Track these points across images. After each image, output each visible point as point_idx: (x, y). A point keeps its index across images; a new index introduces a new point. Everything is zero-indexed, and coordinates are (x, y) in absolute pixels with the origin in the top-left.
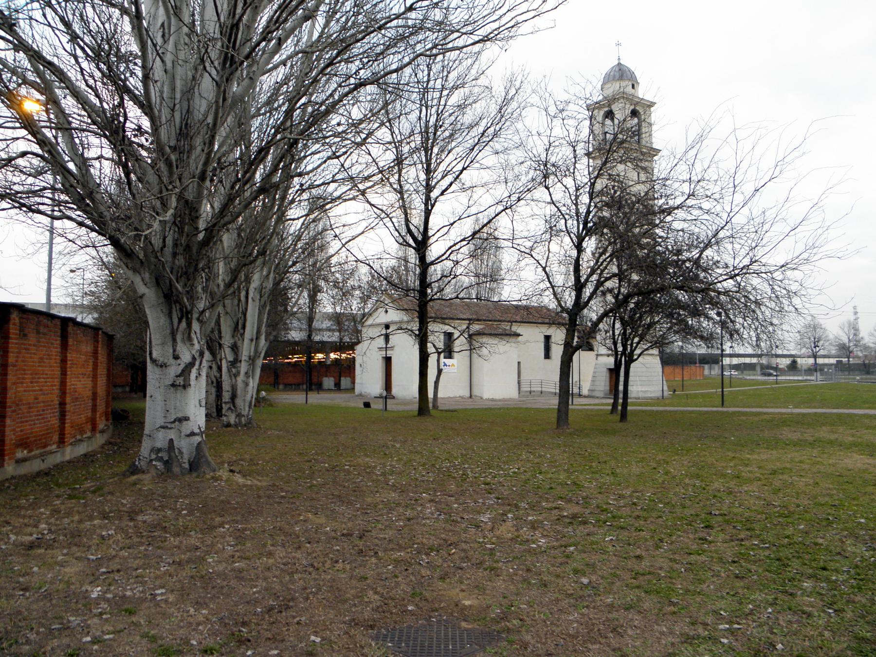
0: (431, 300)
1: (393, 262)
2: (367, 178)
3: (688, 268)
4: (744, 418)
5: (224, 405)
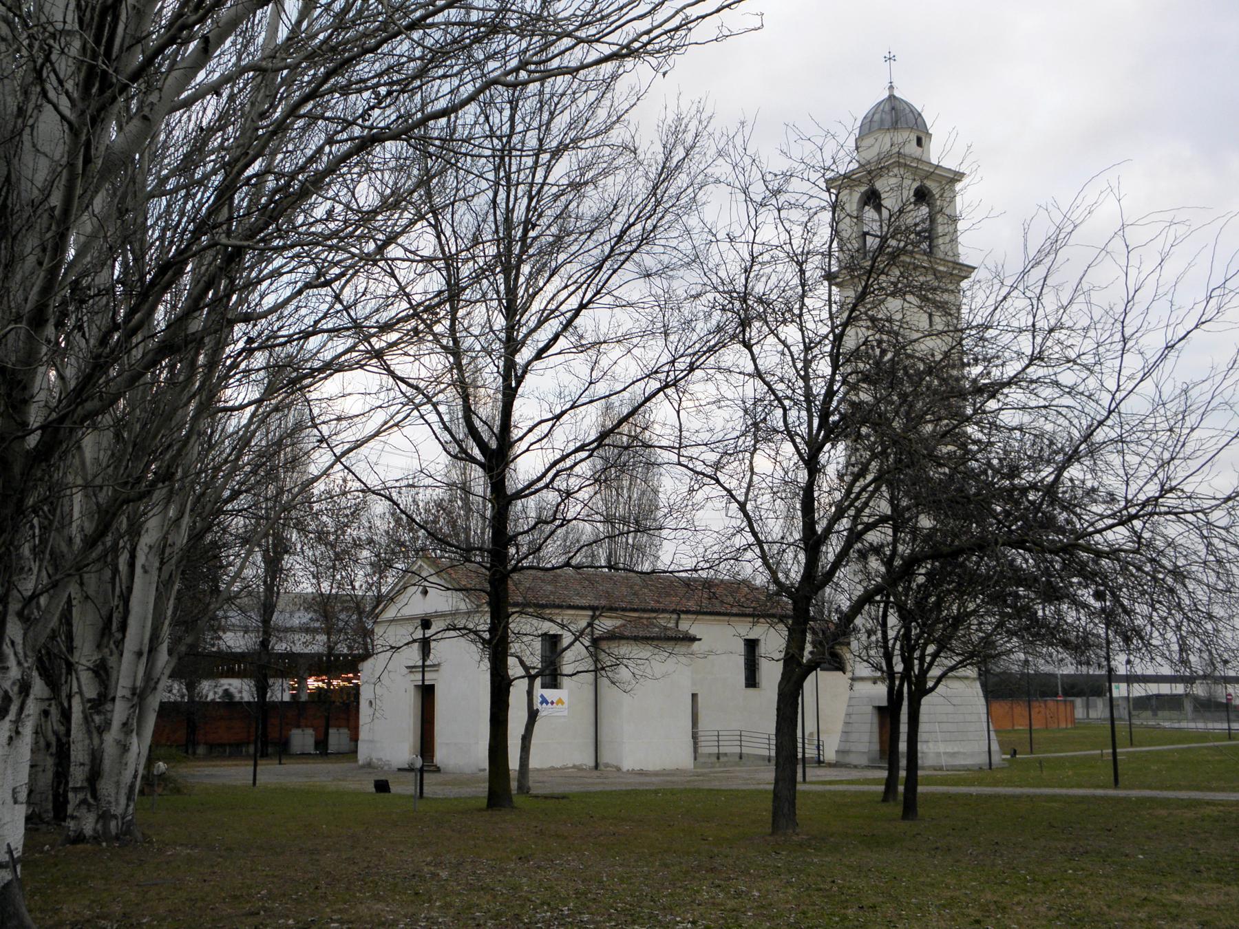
0: (516, 569)
1: (439, 493)
2: (386, 328)
3: (1032, 503)
4: (1164, 812)
5: (71, 795)
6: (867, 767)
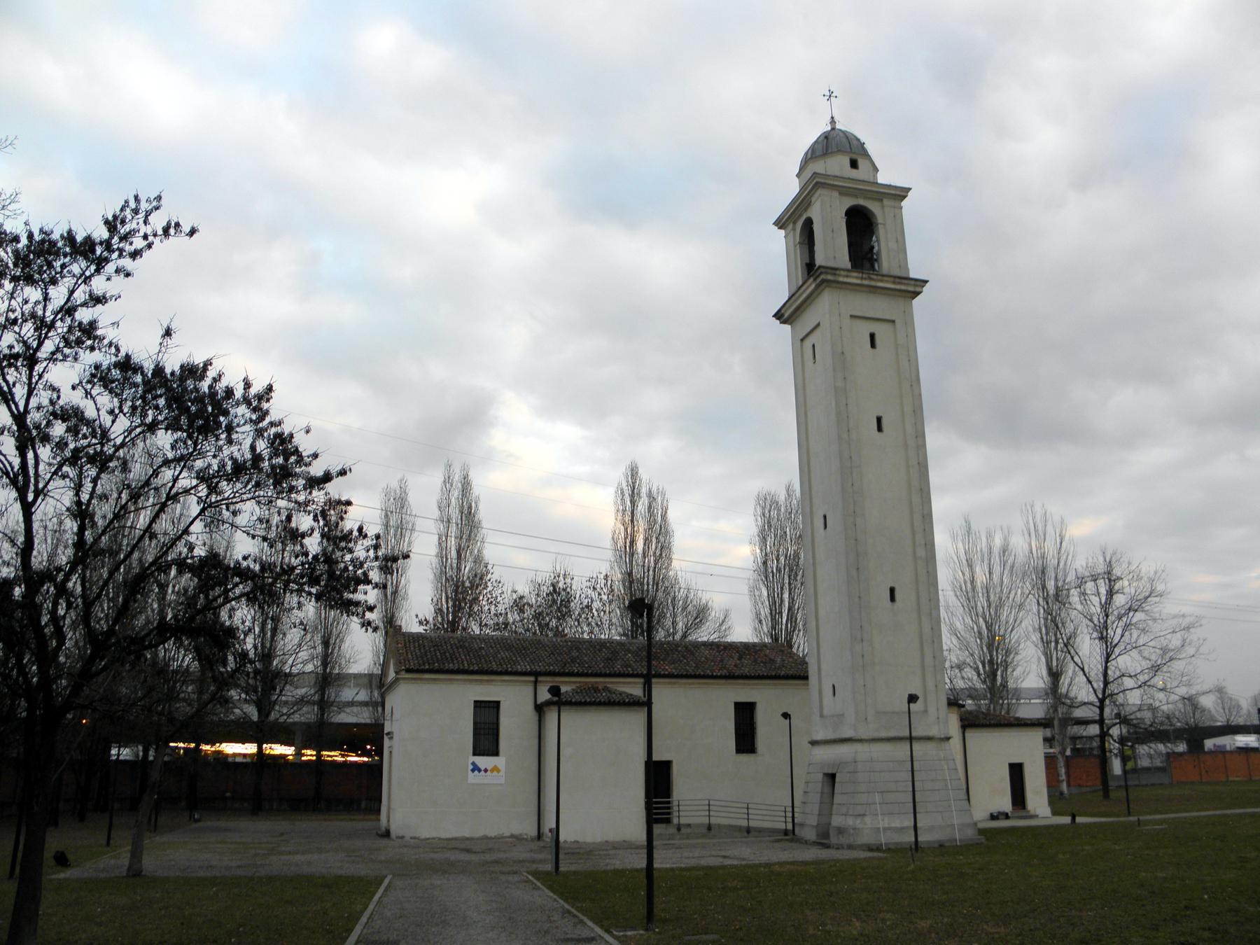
6: (815, 843)
